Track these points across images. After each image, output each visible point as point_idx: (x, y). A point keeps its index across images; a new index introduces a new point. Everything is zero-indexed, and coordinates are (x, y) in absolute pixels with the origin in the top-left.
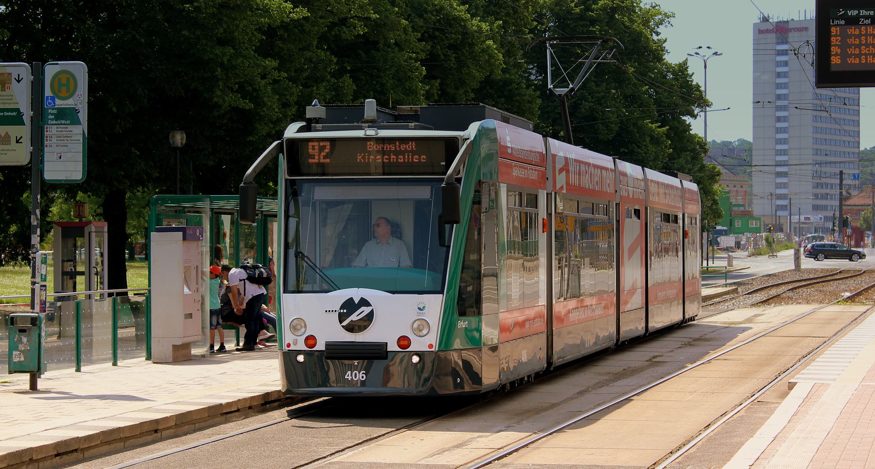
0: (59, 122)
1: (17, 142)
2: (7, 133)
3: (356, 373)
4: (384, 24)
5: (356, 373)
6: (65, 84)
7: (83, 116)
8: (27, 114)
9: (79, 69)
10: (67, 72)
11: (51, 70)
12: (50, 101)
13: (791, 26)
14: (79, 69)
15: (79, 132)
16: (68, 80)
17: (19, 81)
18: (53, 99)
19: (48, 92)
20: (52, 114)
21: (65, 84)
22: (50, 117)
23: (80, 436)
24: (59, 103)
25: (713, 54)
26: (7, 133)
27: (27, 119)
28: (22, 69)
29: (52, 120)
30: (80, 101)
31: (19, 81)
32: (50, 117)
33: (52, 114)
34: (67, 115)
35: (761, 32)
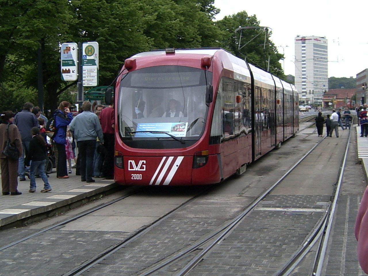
0: (88, 65)
1: (73, 72)
2: (69, 69)
3: (131, 162)
4: (159, 17)
5: (131, 162)
6: (90, 51)
7: (97, 62)
8: (76, 61)
9: (95, 45)
10: (91, 46)
11: (85, 45)
12: (85, 57)
13: (306, 38)
14: (95, 45)
15: (95, 68)
16: (91, 48)
17: (74, 50)
18: (86, 56)
19: (84, 54)
20: (85, 62)
21: (90, 51)
22: (85, 63)
23: (336, 77)
24: (88, 58)
25: (21, 194)
26: (69, 69)
27: (76, 63)
28: (73, 46)
29: (85, 64)
30: (95, 57)
31: (74, 50)
32: (85, 63)
33: (85, 62)
34: (92, 62)
35: (297, 40)
